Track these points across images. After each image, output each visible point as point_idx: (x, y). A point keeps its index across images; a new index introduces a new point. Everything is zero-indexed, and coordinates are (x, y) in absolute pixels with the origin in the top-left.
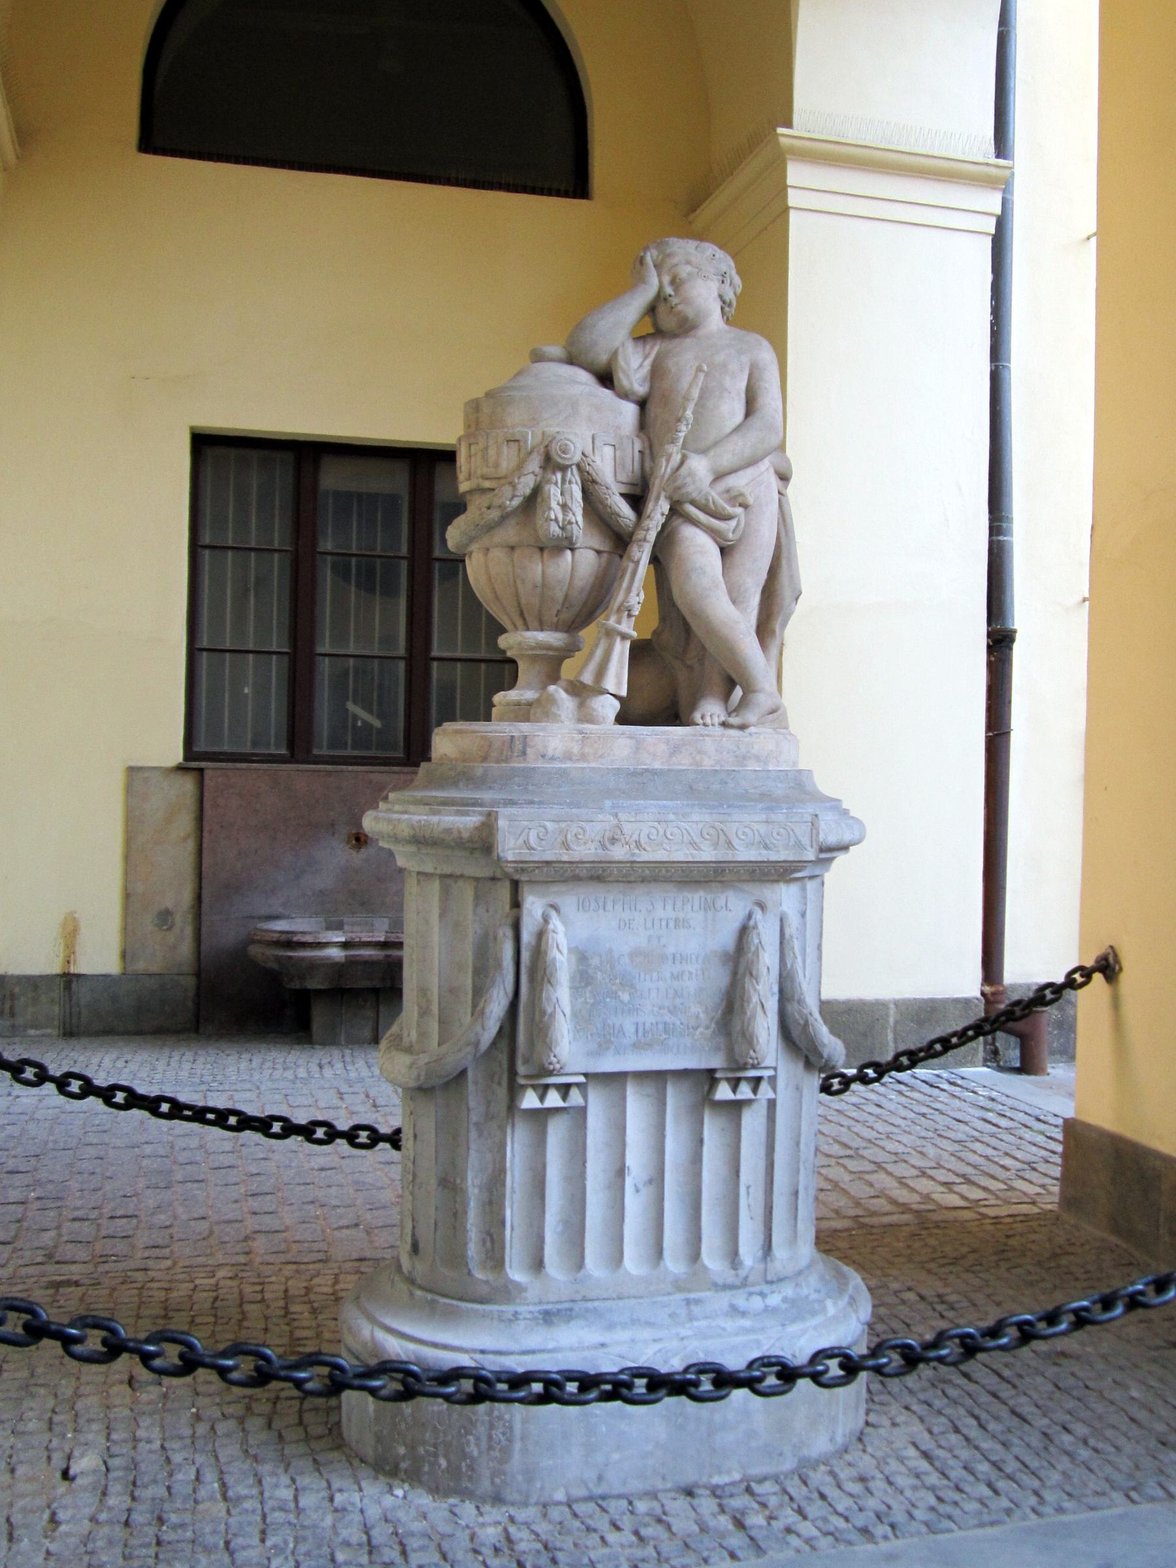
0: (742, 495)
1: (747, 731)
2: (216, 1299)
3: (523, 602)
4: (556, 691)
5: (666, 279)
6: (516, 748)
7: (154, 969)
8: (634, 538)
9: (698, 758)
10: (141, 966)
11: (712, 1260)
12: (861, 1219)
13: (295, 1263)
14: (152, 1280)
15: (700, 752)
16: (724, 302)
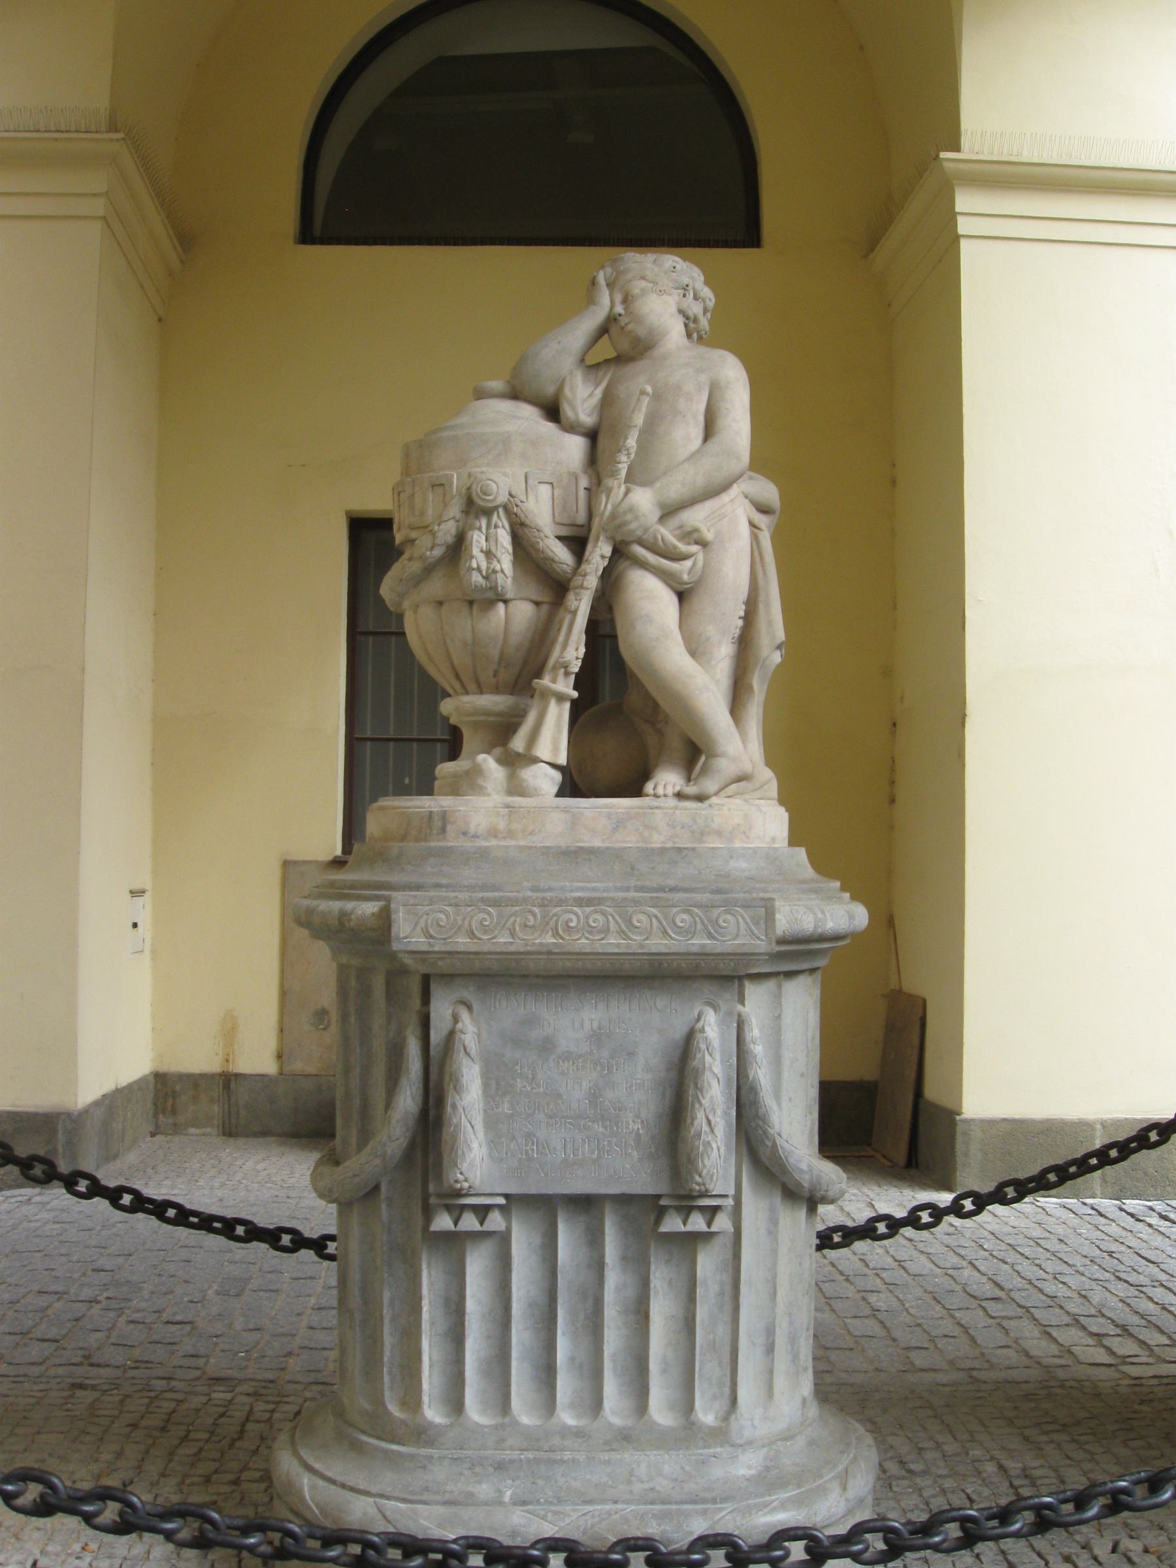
0: (696, 530)
1: (707, 803)
2: (223, 1415)
3: (456, 663)
4: (485, 760)
5: (618, 298)
6: (441, 823)
7: (311, 1069)
8: (572, 585)
9: (646, 833)
10: (298, 1066)
11: (660, 1412)
12: (974, 1373)
13: (323, 1383)
14: (171, 1390)
15: (647, 827)
16: (688, 318)
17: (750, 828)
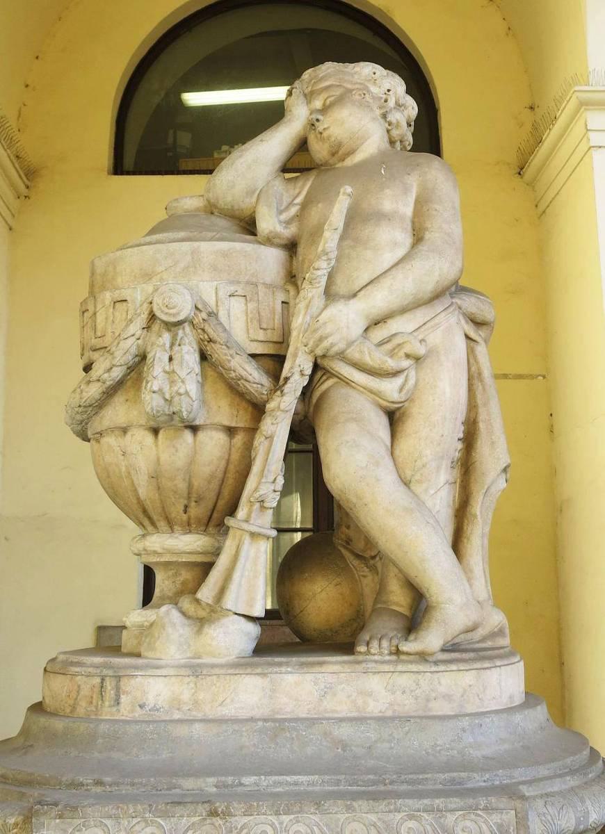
17: (485, 688)
